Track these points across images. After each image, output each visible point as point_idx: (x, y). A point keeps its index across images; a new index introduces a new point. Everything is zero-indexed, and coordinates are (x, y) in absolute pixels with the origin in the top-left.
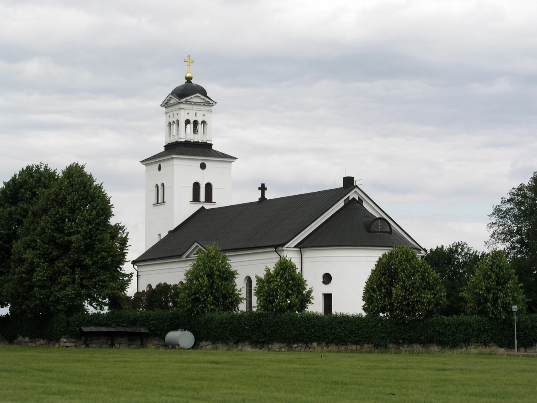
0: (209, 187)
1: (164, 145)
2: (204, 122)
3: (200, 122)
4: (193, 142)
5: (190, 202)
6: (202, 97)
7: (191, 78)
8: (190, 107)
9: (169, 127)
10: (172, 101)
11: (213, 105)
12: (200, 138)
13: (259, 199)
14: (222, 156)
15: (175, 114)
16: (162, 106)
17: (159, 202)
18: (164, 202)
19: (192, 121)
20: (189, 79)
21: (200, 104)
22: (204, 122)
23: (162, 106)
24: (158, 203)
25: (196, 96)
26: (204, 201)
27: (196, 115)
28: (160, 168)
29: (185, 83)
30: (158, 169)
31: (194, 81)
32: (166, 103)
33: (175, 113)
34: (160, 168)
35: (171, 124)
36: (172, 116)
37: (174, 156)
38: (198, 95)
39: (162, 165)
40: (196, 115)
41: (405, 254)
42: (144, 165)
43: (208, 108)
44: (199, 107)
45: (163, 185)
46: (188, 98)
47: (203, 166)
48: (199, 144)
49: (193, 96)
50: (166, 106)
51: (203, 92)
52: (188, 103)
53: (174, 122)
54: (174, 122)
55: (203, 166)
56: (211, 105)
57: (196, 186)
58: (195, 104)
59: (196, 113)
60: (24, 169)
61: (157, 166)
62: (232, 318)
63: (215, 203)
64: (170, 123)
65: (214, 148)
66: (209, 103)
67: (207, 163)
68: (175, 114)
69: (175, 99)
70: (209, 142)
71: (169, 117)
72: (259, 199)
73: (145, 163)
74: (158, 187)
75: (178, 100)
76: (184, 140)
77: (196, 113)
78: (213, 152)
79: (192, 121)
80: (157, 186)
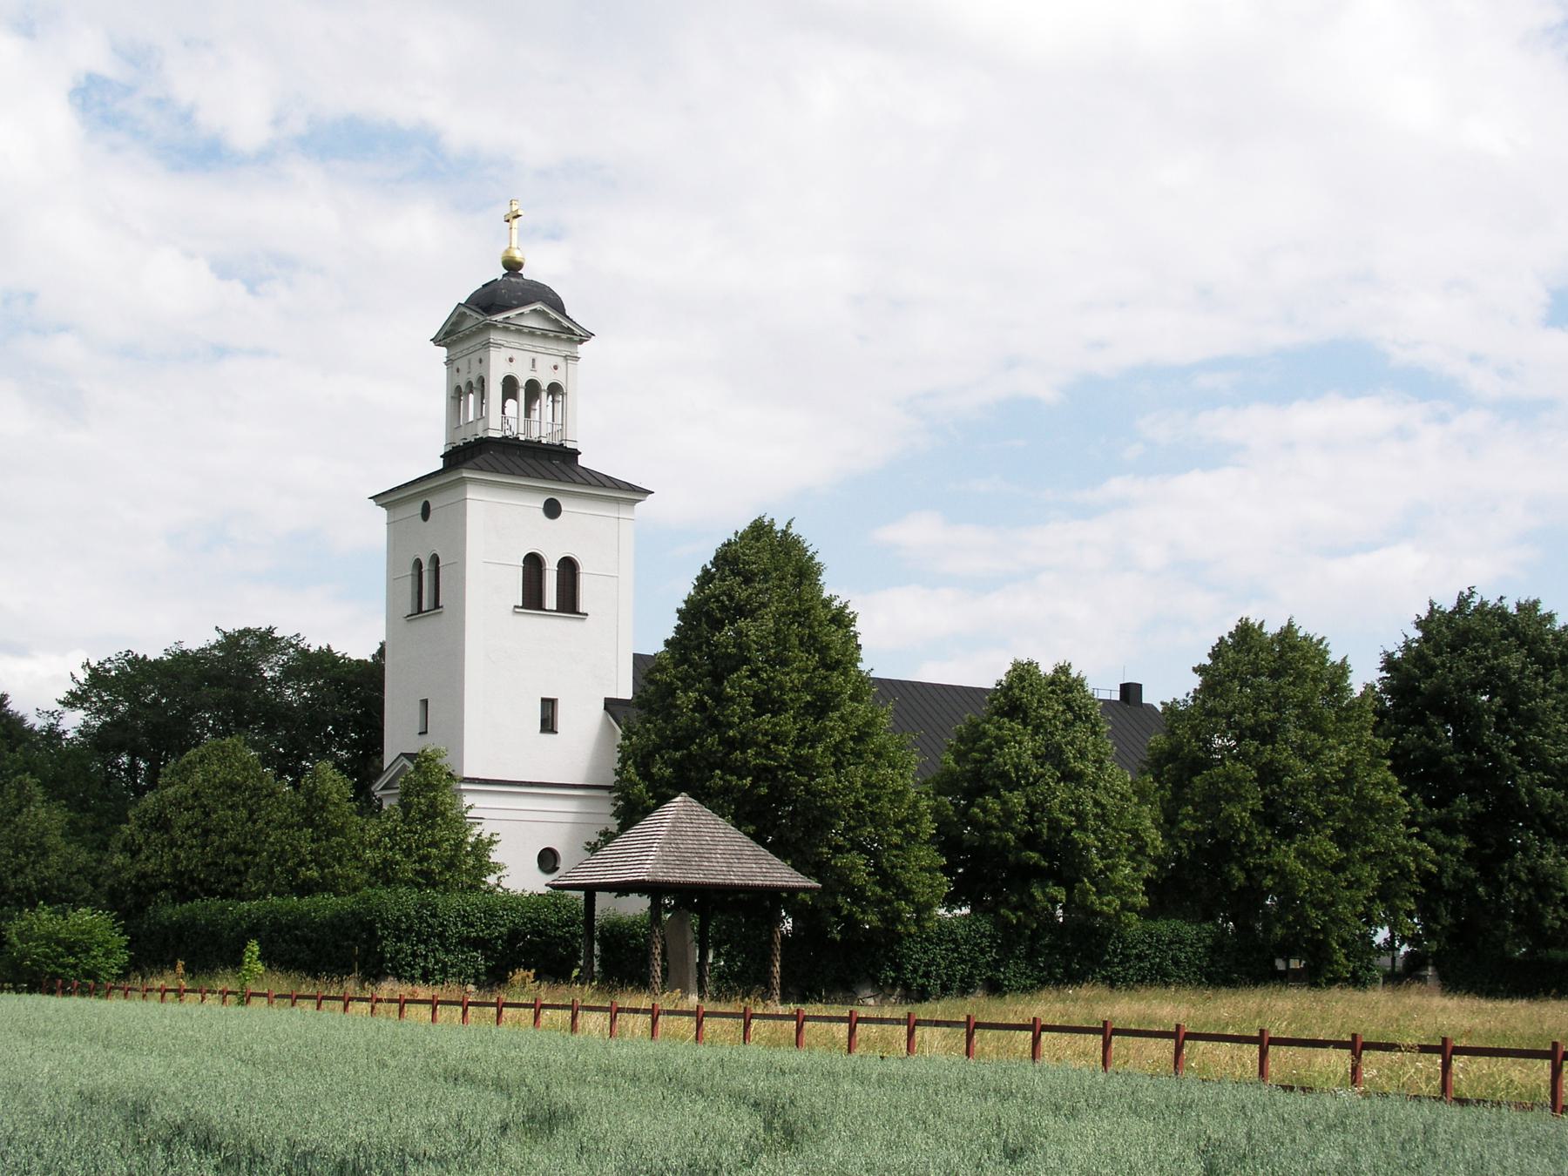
0: (568, 568)
1: (442, 453)
2: (555, 389)
3: (544, 386)
4: (526, 441)
5: (516, 607)
6: (554, 315)
7: (520, 265)
8: (513, 340)
9: (457, 401)
10: (468, 324)
11: (581, 342)
12: (542, 426)
13: (641, 662)
14: (608, 483)
15: (475, 363)
16: (437, 341)
17: (425, 607)
18: (437, 606)
19: (522, 382)
20: (512, 266)
21: (532, 333)
22: (555, 389)
23: (437, 341)
24: (420, 611)
25: (535, 310)
26: (555, 608)
27: (533, 366)
28: (426, 513)
29: (504, 275)
30: (420, 516)
31: (527, 273)
32: (448, 334)
33: (475, 357)
34: (426, 513)
35: (463, 390)
36: (463, 368)
37: (466, 474)
38: (538, 306)
39: (434, 504)
40: (533, 366)
41: (976, 761)
42: (382, 505)
43: (565, 349)
44: (539, 344)
45: (435, 560)
46: (512, 314)
47: (552, 510)
48: (539, 448)
49: (526, 310)
50: (448, 340)
51: (558, 306)
52: (513, 328)
53: (470, 384)
54: (470, 384)
55: (552, 510)
56: (576, 338)
57: (533, 563)
58: (520, 331)
59: (534, 360)
60: (615, 894)
61: (417, 508)
62: (308, 670)
63: (587, 615)
64: (458, 388)
65: (582, 461)
66: (569, 334)
67: (566, 505)
68: (475, 363)
69: (475, 315)
70: (569, 445)
71: (458, 370)
72: (641, 662)
73: (384, 501)
74: (420, 566)
75: (481, 318)
76: (498, 435)
77: (534, 360)
78: (578, 470)
79: (522, 382)
80: (418, 564)
